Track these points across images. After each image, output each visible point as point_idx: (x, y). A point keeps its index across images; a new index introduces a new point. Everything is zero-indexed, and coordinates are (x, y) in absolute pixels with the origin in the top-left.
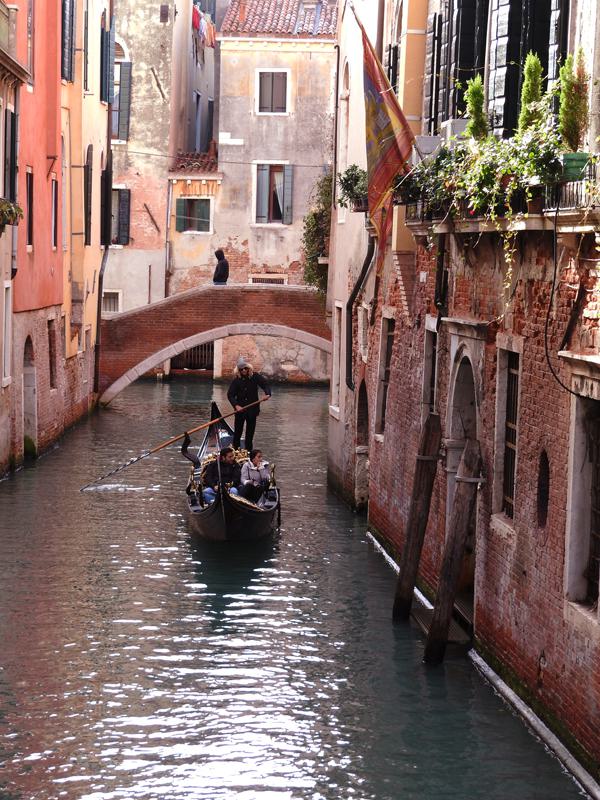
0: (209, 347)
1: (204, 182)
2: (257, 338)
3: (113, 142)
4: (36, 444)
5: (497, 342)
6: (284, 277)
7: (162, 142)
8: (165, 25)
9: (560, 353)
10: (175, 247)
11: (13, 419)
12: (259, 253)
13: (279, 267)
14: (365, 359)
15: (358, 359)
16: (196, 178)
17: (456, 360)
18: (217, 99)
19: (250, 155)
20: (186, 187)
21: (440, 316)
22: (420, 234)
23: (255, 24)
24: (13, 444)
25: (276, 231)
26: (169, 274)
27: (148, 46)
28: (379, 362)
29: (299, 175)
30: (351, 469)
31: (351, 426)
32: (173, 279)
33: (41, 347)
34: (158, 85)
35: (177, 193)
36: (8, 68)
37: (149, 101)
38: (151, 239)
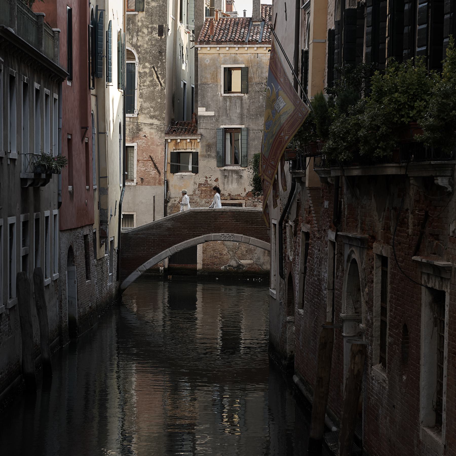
0: (194, 249)
1: (188, 141)
2: (226, 242)
3: (127, 115)
4: (77, 317)
5: (374, 249)
6: (243, 202)
7: (160, 115)
8: (161, 38)
9: (414, 258)
10: (170, 184)
11: (61, 301)
12: (226, 186)
13: (239, 195)
14: (291, 258)
15: (287, 258)
16: (183, 138)
17: (348, 261)
18: (196, 86)
19: (219, 122)
20: (177, 144)
21: (337, 231)
22: (323, 176)
23: (221, 36)
24: (61, 317)
25: (237, 172)
26: (166, 202)
27: (150, 52)
28: (300, 260)
29: (251, 135)
30: (284, 332)
31: (283, 303)
32: (169, 204)
33: (79, 254)
34: (158, 78)
35: (171, 148)
36: (53, 70)
37: (152, 88)
38: (154, 178)
